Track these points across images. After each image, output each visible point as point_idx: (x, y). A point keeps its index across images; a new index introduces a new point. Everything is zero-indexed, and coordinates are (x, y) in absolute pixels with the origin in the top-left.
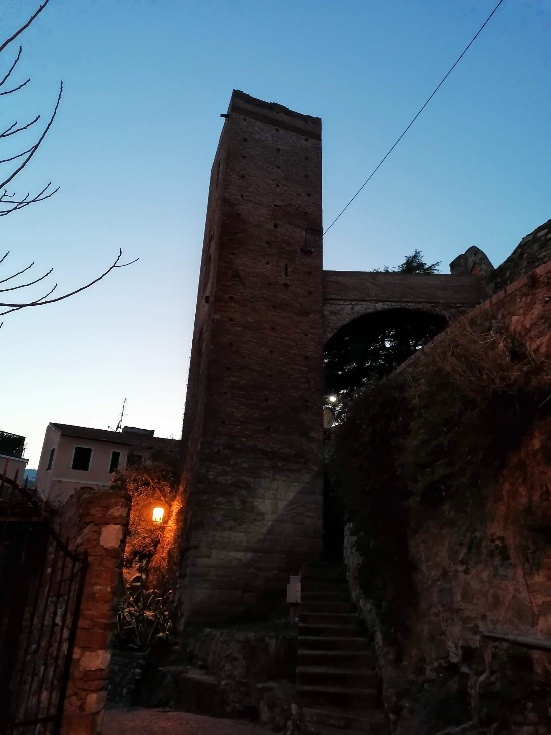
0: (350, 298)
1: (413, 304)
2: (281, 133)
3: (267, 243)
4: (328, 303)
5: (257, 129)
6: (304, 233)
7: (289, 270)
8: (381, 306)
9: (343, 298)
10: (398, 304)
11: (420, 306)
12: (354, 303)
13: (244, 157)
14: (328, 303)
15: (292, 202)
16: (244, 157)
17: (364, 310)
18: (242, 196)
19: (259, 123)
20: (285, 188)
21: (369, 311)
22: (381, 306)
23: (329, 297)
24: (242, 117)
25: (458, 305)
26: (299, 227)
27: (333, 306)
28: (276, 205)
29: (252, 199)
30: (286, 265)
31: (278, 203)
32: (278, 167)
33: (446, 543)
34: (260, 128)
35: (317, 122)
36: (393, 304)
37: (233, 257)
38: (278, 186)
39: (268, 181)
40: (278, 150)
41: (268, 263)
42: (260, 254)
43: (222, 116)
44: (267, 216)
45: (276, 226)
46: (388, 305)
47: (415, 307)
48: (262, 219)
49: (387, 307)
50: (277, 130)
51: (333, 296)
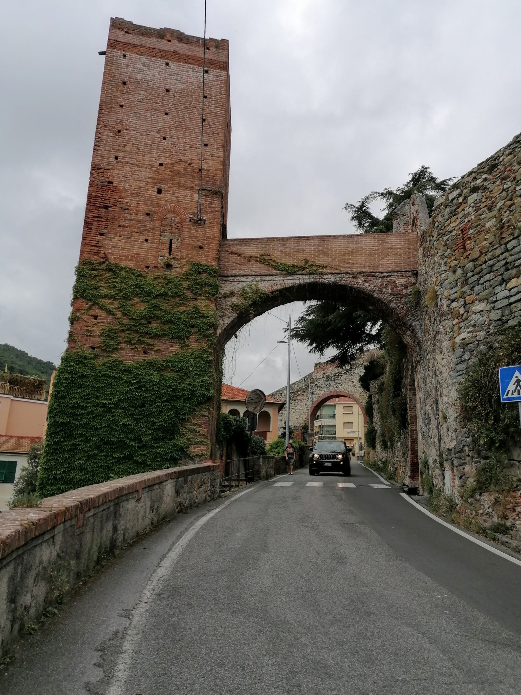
0: (254, 273)
1: (330, 276)
2: (172, 67)
3: (148, 214)
4: (228, 281)
5: (140, 66)
6: (196, 196)
7: (174, 246)
8: (291, 281)
9: (246, 274)
10: (312, 276)
11: (338, 278)
12: (259, 278)
13: (122, 106)
14: (228, 281)
15: (182, 158)
16: (122, 106)
17: (270, 287)
18: (116, 158)
19: (144, 59)
20: (174, 140)
21: (275, 288)
22: (291, 281)
23: (229, 273)
24: (120, 53)
25: (386, 274)
26: (190, 188)
27: (233, 283)
28: (161, 165)
29: (127, 160)
30: (171, 240)
31: (164, 161)
32: (167, 114)
33: (505, 423)
34: (143, 64)
35: (222, 45)
36: (305, 277)
37: (100, 238)
38: (164, 139)
39: (152, 133)
40: (168, 91)
41: (146, 240)
42: (136, 230)
43: (101, 53)
44: (150, 180)
45: (159, 191)
46: (299, 279)
47: (332, 279)
48: (141, 185)
49: (297, 282)
50: (167, 64)
51: (234, 272)
